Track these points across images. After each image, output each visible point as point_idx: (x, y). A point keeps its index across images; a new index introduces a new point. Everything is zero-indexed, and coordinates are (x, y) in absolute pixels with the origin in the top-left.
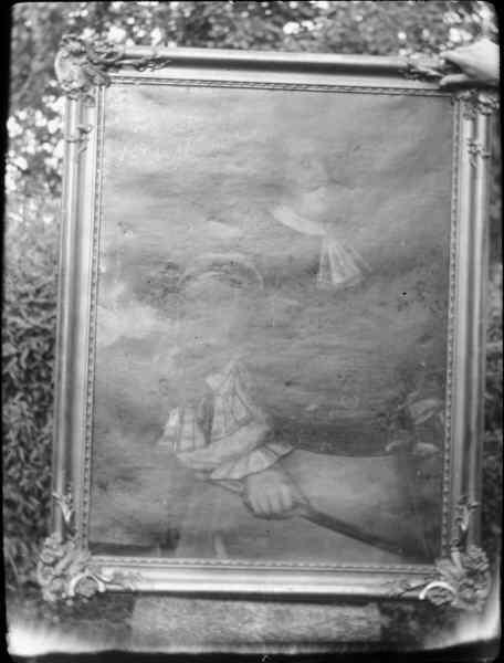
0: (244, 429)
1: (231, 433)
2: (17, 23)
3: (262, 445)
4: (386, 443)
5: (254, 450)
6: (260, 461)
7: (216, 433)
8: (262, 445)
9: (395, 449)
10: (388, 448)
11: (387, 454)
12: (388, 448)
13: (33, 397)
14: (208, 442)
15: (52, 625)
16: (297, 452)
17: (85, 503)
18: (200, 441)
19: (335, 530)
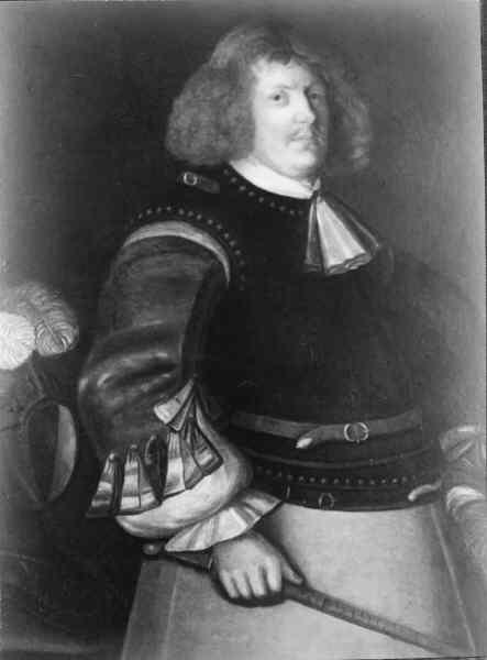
0: (208, 479)
1: (190, 485)
2: (213, 74)
3: (236, 499)
4: (408, 493)
5: (226, 507)
6: (233, 523)
7: (171, 485)
8: (236, 499)
9: (419, 501)
10: (412, 497)
11: (410, 505)
12: (412, 497)
13: (222, 97)
14: (160, 497)
15: (168, 153)
16: (286, 506)
17: (22, 409)
18: (148, 499)
19: (76, 427)
